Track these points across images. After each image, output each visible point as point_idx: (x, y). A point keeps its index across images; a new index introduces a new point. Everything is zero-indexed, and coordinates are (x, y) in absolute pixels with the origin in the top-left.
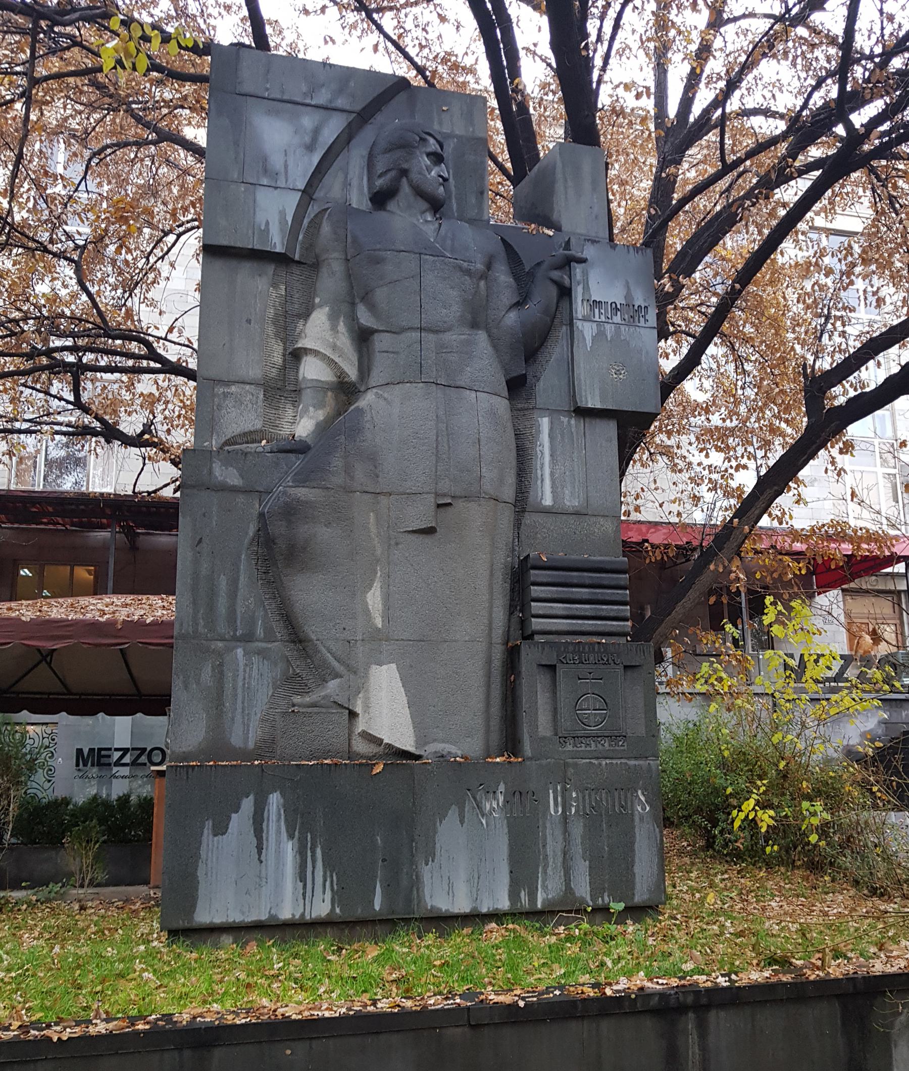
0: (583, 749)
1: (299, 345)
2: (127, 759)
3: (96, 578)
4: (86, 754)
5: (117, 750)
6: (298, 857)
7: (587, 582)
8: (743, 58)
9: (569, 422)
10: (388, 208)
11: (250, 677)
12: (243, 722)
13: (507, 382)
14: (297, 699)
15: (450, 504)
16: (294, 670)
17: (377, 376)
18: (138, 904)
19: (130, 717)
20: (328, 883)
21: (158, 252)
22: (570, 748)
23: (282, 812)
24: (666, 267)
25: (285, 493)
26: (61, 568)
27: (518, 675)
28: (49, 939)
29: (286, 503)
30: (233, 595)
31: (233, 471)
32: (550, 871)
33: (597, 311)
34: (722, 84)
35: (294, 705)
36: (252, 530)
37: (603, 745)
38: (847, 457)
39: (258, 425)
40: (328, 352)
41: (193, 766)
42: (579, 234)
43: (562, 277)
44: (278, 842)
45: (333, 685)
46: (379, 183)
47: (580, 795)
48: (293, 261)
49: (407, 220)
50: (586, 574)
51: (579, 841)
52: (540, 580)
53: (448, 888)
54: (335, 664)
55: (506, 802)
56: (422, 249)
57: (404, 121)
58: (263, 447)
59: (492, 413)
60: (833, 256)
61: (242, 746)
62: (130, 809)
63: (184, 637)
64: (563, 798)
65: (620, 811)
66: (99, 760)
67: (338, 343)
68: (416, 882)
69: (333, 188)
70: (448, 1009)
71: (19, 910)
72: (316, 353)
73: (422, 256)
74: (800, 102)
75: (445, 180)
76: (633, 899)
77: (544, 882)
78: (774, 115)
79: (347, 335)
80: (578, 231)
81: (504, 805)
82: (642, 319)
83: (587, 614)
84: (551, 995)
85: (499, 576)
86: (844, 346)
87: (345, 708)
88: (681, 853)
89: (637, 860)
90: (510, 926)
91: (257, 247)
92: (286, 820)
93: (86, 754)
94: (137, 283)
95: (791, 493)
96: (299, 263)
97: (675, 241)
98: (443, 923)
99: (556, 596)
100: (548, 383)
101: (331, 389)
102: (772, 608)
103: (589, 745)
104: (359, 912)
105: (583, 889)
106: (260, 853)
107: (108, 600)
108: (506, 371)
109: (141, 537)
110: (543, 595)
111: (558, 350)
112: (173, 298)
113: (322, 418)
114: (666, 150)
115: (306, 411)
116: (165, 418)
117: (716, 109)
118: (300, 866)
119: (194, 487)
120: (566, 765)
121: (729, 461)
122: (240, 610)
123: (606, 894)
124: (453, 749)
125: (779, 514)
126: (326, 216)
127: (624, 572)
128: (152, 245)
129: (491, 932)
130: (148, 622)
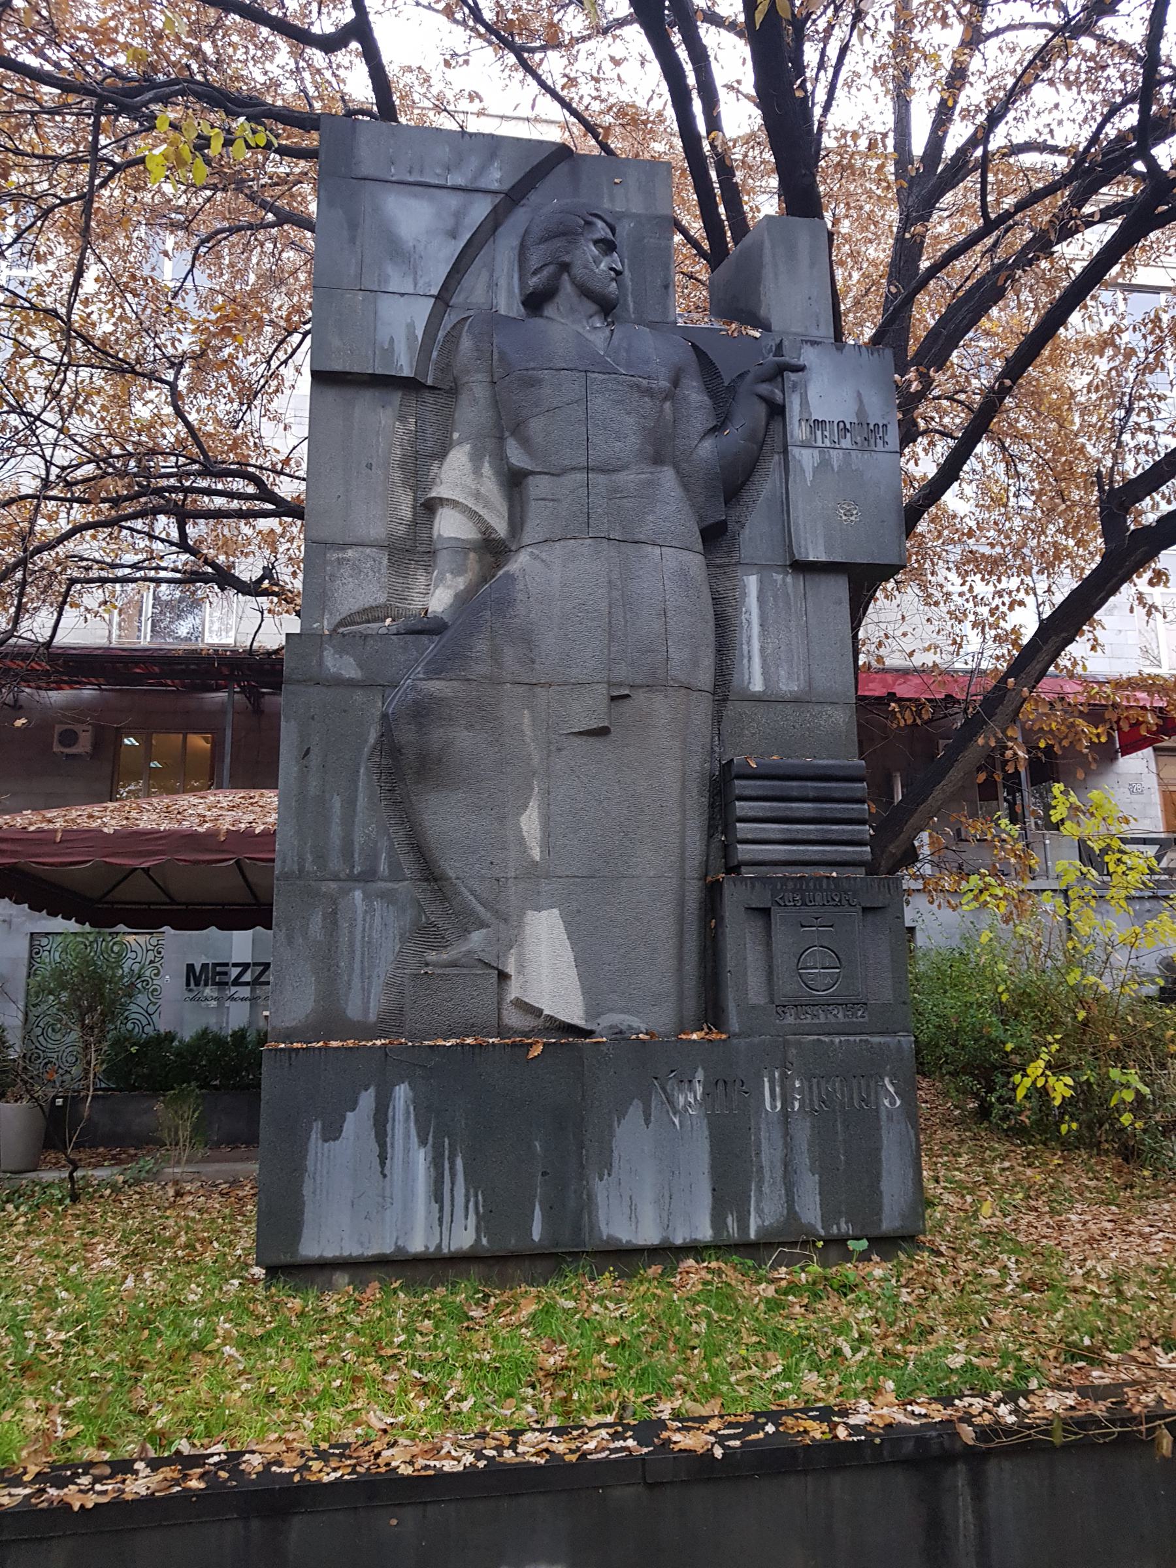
1: (433, 494)
2: (247, 977)
4: (198, 970)
7: (811, 794)
8: (1010, 81)
9: (784, 580)
10: (546, 313)
11: (371, 927)
12: (363, 989)
13: (701, 531)
14: (432, 956)
15: (627, 696)
17: (533, 530)
20: (471, 1205)
21: (282, 355)
22: (790, 1020)
24: (909, 353)
25: (414, 687)
26: (173, 736)
27: (720, 920)
28: (126, 1257)
30: (348, 820)
32: (766, 1189)
33: (819, 433)
34: (981, 118)
35: (427, 965)
36: (373, 737)
38: (1159, 589)
39: (382, 598)
40: (470, 503)
43: (773, 392)
44: (407, 1150)
46: (533, 281)
47: (806, 1084)
49: (569, 327)
50: (809, 784)
51: (805, 1147)
52: (747, 793)
53: (630, 1212)
54: (481, 910)
55: (706, 1094)
56: (589, 365)
59: (683, 575)
60: (1134, 330)
66: (213, 978)
67: (482, 490)
68: (587, 1204)
69: (473, 291)
70: (615, 1460)
71: (101, 1196)
72: (454, 504)
74: (1087, 132)
77: (758, 1202)
78: (1054, 150)
80: (793, 330)
83: (812, 837)
84: (761, 1435)
85: (694, 786)
86: (1151, 446)
88: (947, 1122)
89: (884, 1174)
90: (714, 1265)
91: (379, 371)
92: (417, 1121)
93: (198, 970)
94: (256, 394)
95: (1085, 638)
96: (432, 388)
97: (927, 313)
98: (625, 1259)
99: (769, 814)
100: (754, 532)
101: (474, 550)
102: (1062, 798)
103: (816, 1016)
104: (513, 1244)
105: (811, 1213)
108: (700, 519)
110: (751, 814)
112: (284, 426)
115: (441, 579)
116: (290, 559)
117: (975, 147)
119: (299, 682)
120: (786, 1044)
122: (359, 839)
124: (635, 1022)
125: (1068, 664)
127: (861, 780)
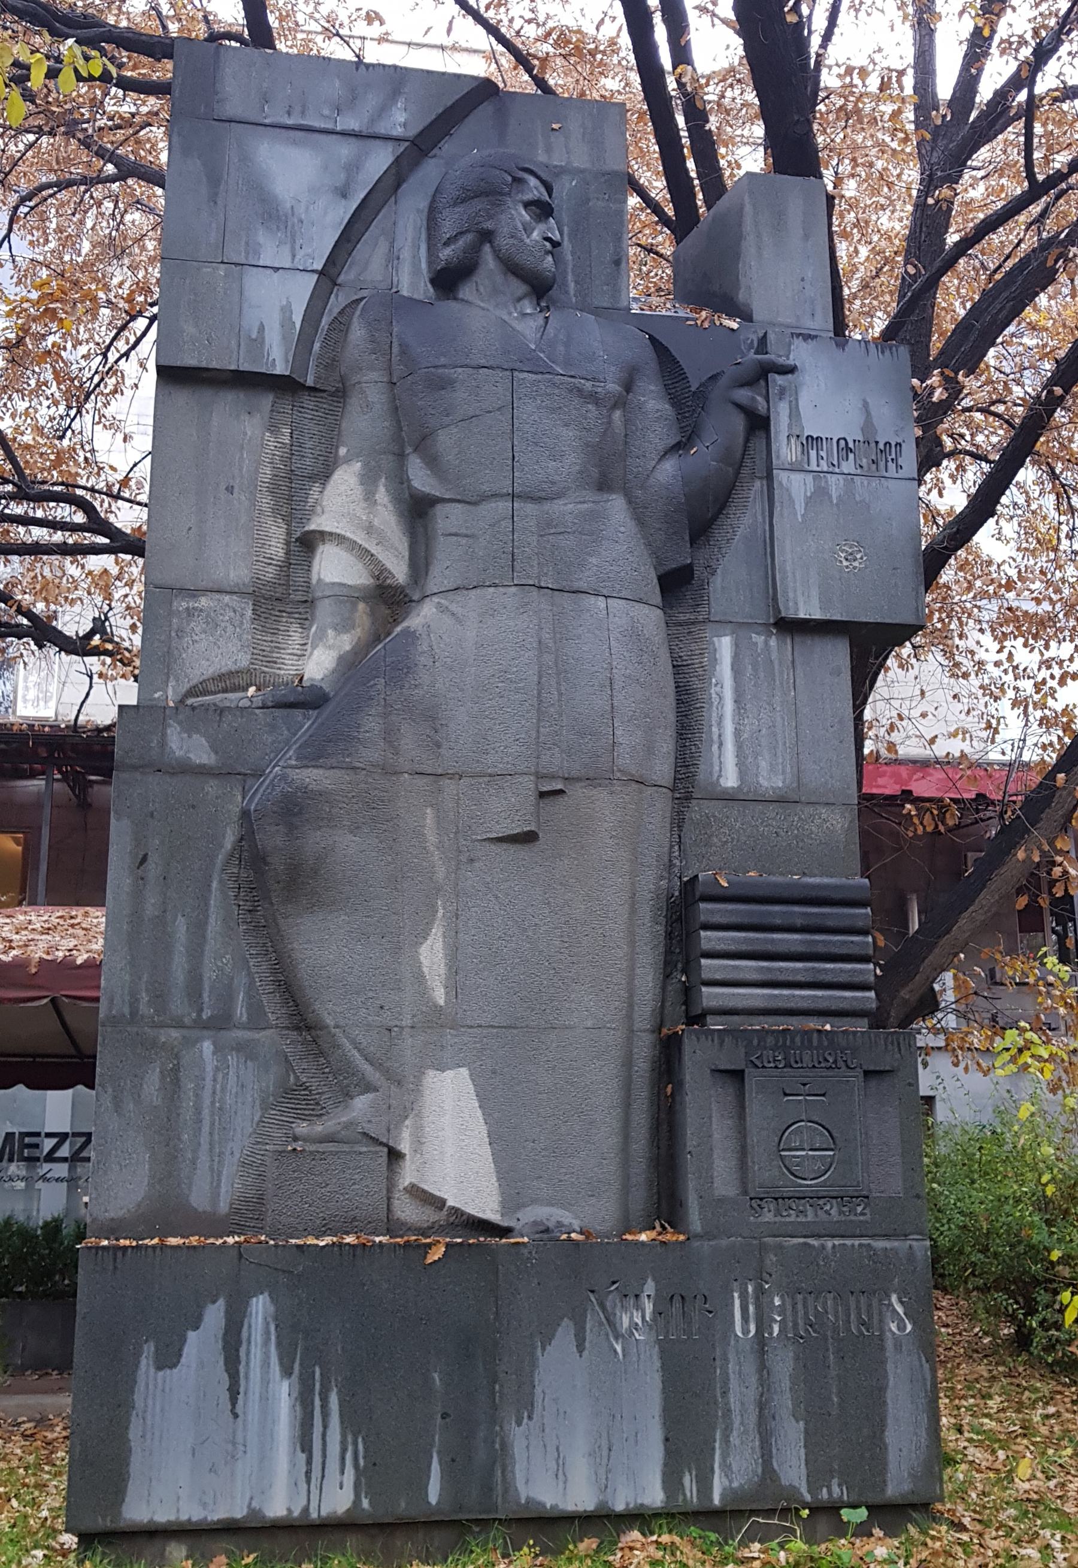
0: (792, 1219)
1: (312, 527)
2: (64, 1151)
3: (26, 850)
5: (49, 1135)
6: (298, 1408)
7: (799, 922)
9: (766, 643)
10: (461, 296)
11: (223, 1089)
14: (302, 1128)
15: (561, 792)
16: (297, 1078)
17: (439, 577)
18: (58, 1429)
19: (70, 1091)
20: (349, 1456)
21: (122, 346)
22: (768, 1217)
23: (272, 1328)
25: (284, 777)
27: (679, 1085)
29: (285, 795)
31: (199, 740)
32: (734, 1439)
34: (1026, 52)
35: (296, 1139)
36: (229, 840)
37: (828, 1213)
40: (360, 538)
41: (125, 1248)
42: (781, 325)
43: (753, 399)
45: (361, 1103)
46: (446, 253)
47: (788, 1301)
48: (303, 387)
49: (491, 312)
50: (796, 909)
51: (786, 1384)
54: (366, 1068)
55: (658, 1313)
56: (519, 362)
57: (486, 152)
58: (250, 699)
61: (208, 1209)
62: (62, 1243)
63: (114, 1021)
64: (758, 1307)
65: (859, 1331)
67: (376, 522)
68: (500, 1456)
69: (370, 265)
72: (339, 539)
73: (516, 373)
75: (556, 244)
76: (883, 1490)
77: (725, 1456)
79: (390, 507)
81: (654, 1320)
82: (892, 466)
85: (646, 912)
87: (382, 1144)
88: (974, 1352)
89: (890, 1421)
90: (665, 1538)
91: (245, 367)
92: (279, 1344)
97: (955, 299)
98: (550, 1527)
99: (744, 948)
100: (729, 581)
101: (364, 599)
104: (403, 1507)
105: (793, 1472)
106: (234, 1400)
107: (22, 918)
108: (658, 563)
109: (96, 787)
110: (721, 947)
111: (747, 520)
113: (348, 648)
114: (934, 160)
115: (321, 636)
116: (128, 608)
117: (1019, 90)
118: (302, 1425)
119: (135, 768)
120: (763, 1248)
121: (1049, 667)
122: (209, 974)
123: (835, 1482)
124: (567, 1217)
126: (358, 313)
127: (863, 904)
128: (112, 334)
129: (631, 1549)
130: (79, 961)
